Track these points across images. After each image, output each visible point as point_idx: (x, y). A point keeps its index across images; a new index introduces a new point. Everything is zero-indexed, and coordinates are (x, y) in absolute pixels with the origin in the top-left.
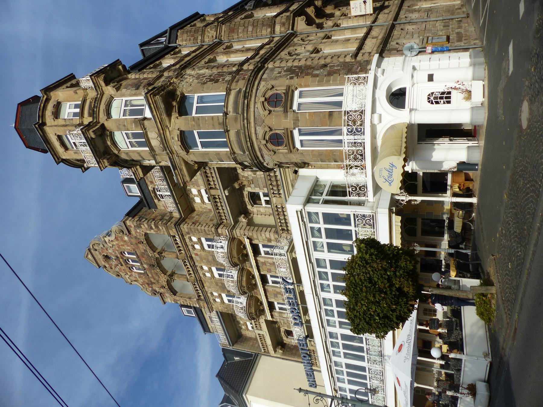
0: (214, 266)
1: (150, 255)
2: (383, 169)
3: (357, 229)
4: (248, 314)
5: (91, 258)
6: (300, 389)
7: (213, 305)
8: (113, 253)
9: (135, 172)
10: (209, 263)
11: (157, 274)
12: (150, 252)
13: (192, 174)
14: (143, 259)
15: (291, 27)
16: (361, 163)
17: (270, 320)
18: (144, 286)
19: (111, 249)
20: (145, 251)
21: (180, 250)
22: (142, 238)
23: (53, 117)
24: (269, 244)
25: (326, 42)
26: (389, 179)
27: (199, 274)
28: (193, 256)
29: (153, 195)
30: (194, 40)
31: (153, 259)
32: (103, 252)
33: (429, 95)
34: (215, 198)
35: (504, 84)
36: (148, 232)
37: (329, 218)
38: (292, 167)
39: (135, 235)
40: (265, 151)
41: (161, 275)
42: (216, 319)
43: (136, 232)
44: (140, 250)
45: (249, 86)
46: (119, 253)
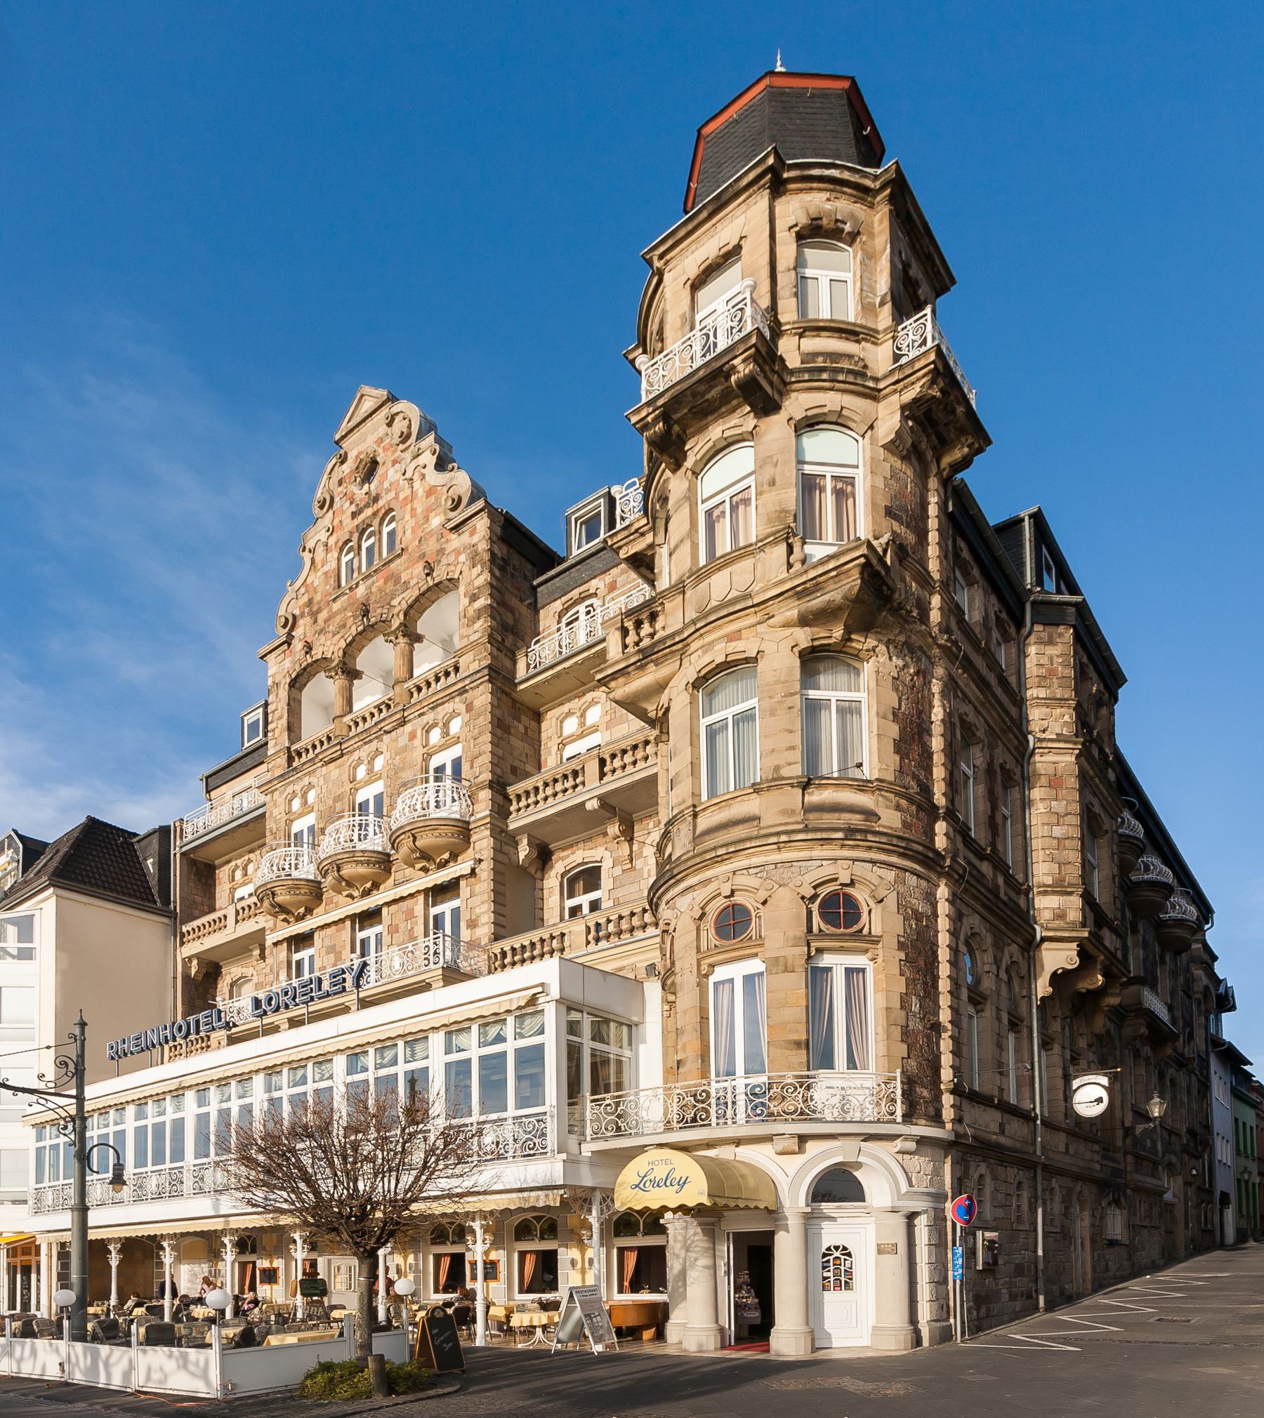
0: (386, 786)
1: (394, 602)
2: (672, 1166)
3: (510, 1121)
4: (269, 886)
5: (363, 411)
6: (86, 1024)
7: (281, 793)
8: (386, 485)
9: (633, 529)
10: (393, 773)
11: (344, 626)
12: (401, 602)
13: (632, 705)
14: (382, 581)
15: (1051, 934)
16: (675, 1120)
17: (265, 940)
18: (303, 590)
19: (399, 475)
20: (406, 586)
21: (419, 689)
22: (440, 574)
23: (804, 220)
24: (463, 925)
25: (1000, 1022)
26: (648, 1183)
27: (359, 748)
28: (408, 727)
29: (575, 594)
30: (1037, 679)
31: (386, 611)
32: (385, 450)
33: (845, 1248)
34: (575, 774)
35: (852, 1388)
36: (462, 589)
37: (531, 1058)
38: (665, 965)
39: (449, 548)
40: (701, 895)
41: (342, 640)
42: (247, 802)
43: (457, 552)
44: (407, 568)
45: (884, 839)
46: (389, 503)
